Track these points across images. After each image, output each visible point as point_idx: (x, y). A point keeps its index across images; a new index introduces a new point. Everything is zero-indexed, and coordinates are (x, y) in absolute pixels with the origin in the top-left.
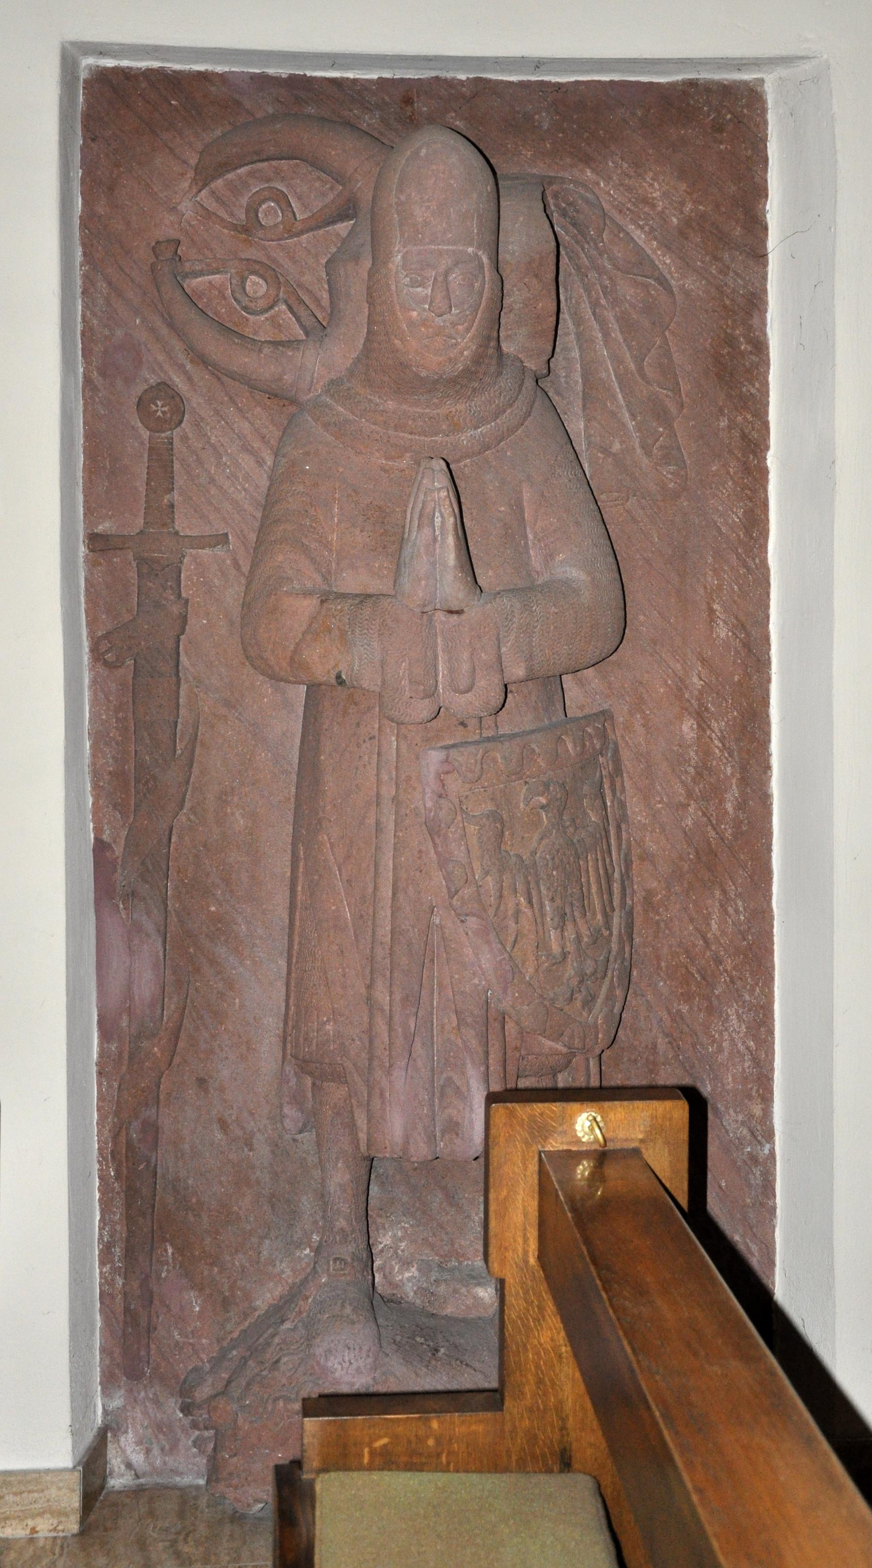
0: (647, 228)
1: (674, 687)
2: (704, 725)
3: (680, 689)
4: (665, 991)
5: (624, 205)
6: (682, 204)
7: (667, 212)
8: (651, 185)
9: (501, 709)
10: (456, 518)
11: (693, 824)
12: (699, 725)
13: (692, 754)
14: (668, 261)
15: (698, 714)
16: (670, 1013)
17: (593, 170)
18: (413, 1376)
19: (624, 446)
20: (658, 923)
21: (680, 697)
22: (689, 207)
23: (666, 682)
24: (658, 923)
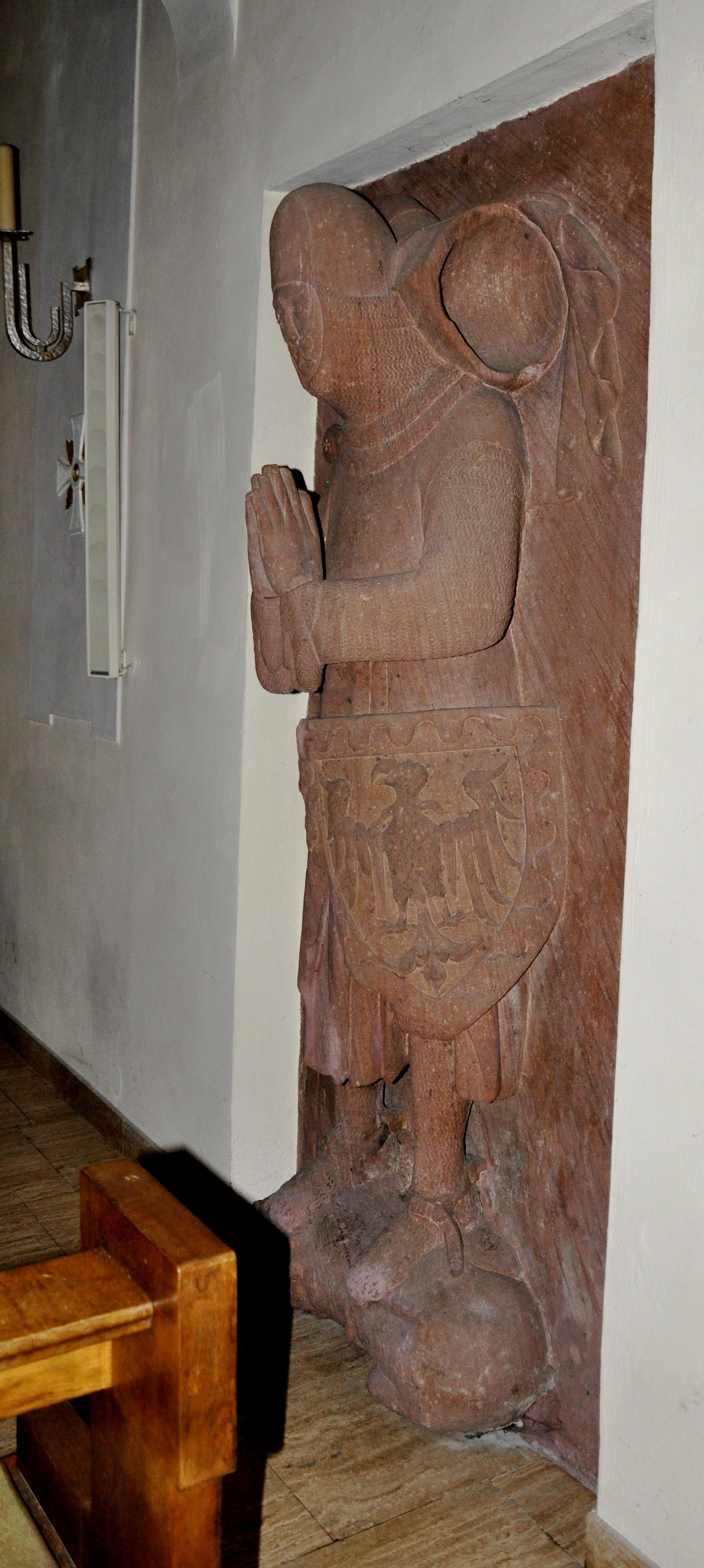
0: (602, 221)
1: (602, 687)
2: (622, 731)
3: (607, 691)
4: (583, 1001)
5: (586, 203)
6: (626, 188)
7: (616, 201)
8: (606, 177)
9: (502, 638)
10: (454, 1555)
11: (610, 834)
12: (618, 730)
13: (613, 760)
14: (615, 250)
15: (619, 718)
16: (584, 1024)
17: (569, 179)
18: (313, 1246)
19: (580, 441)
20: (580, 929)
21: (606, 699)
22: (632, 189)
23: (597, 681)
24: (580, 929)
